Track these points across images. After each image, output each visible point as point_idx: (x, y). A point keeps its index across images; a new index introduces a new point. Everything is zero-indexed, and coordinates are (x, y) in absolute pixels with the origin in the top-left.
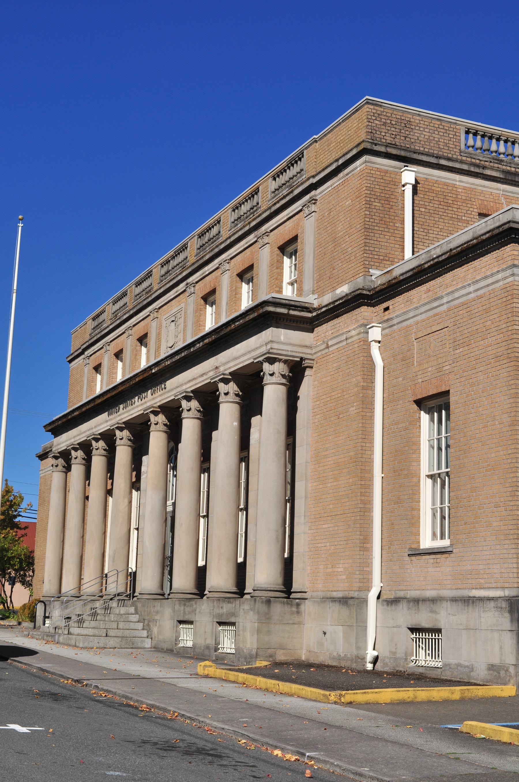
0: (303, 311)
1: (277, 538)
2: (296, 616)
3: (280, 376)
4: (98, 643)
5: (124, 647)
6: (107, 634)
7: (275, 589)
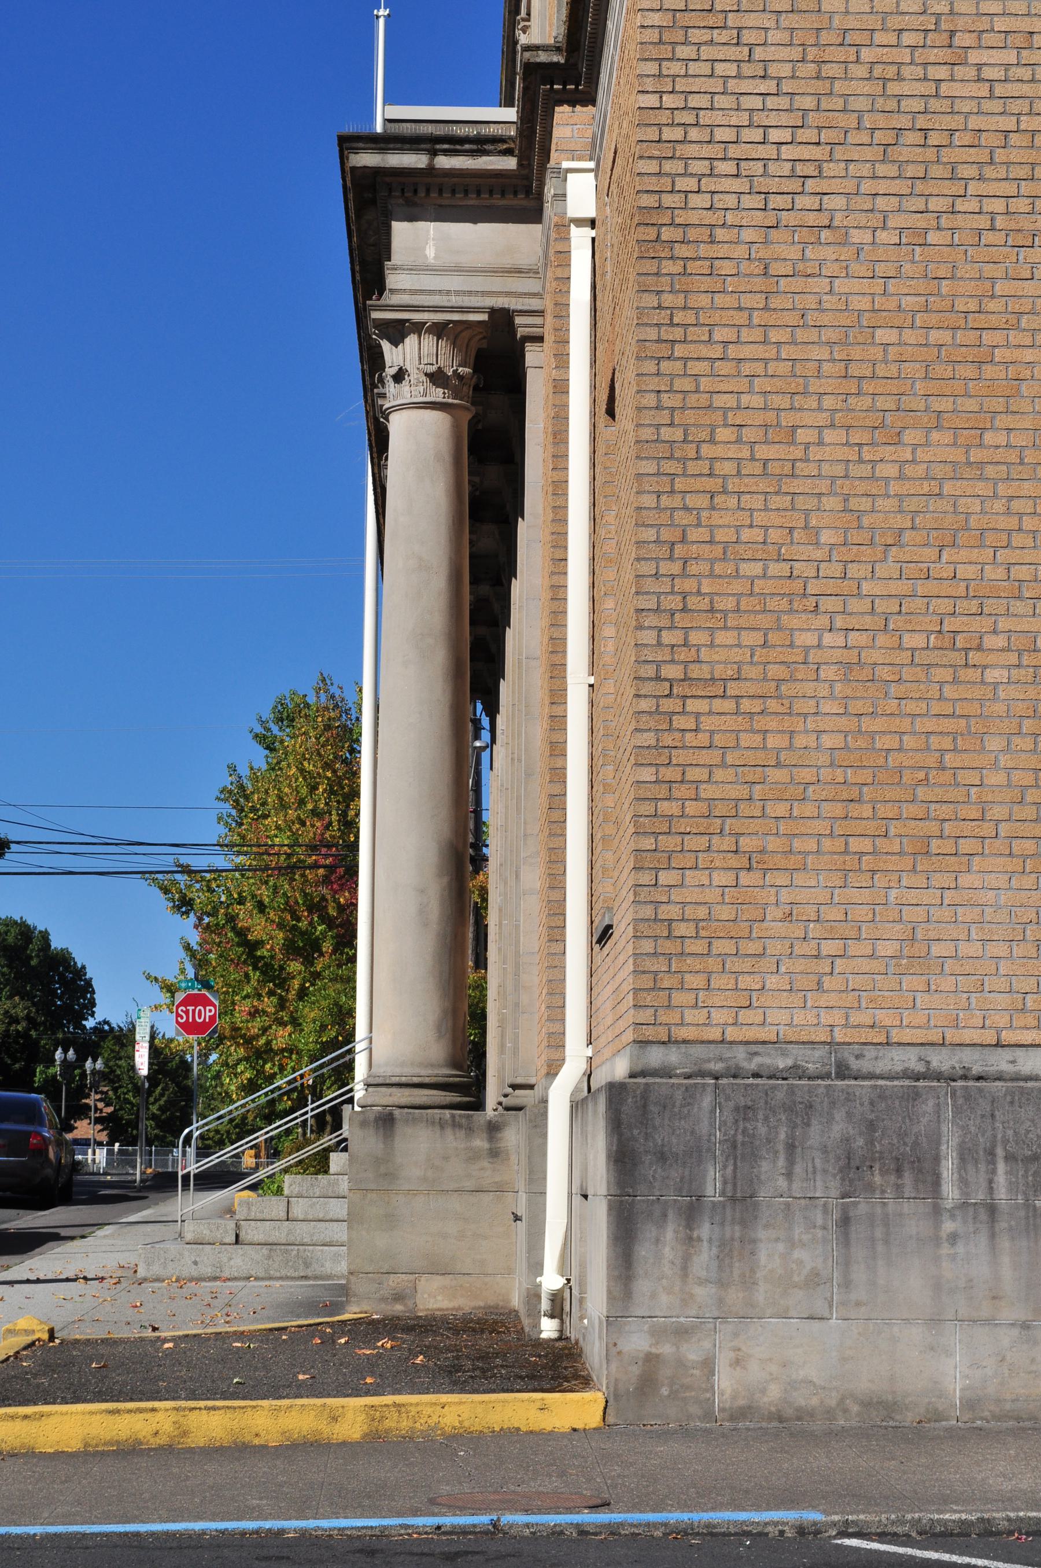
0: (487, 153)
1: (422, 911)
2: (485, 1163)
3: (424, 378)
4: (195, 1263)
5: (278, 1275)
6: (237, 1236)
7: (416, 1080)
